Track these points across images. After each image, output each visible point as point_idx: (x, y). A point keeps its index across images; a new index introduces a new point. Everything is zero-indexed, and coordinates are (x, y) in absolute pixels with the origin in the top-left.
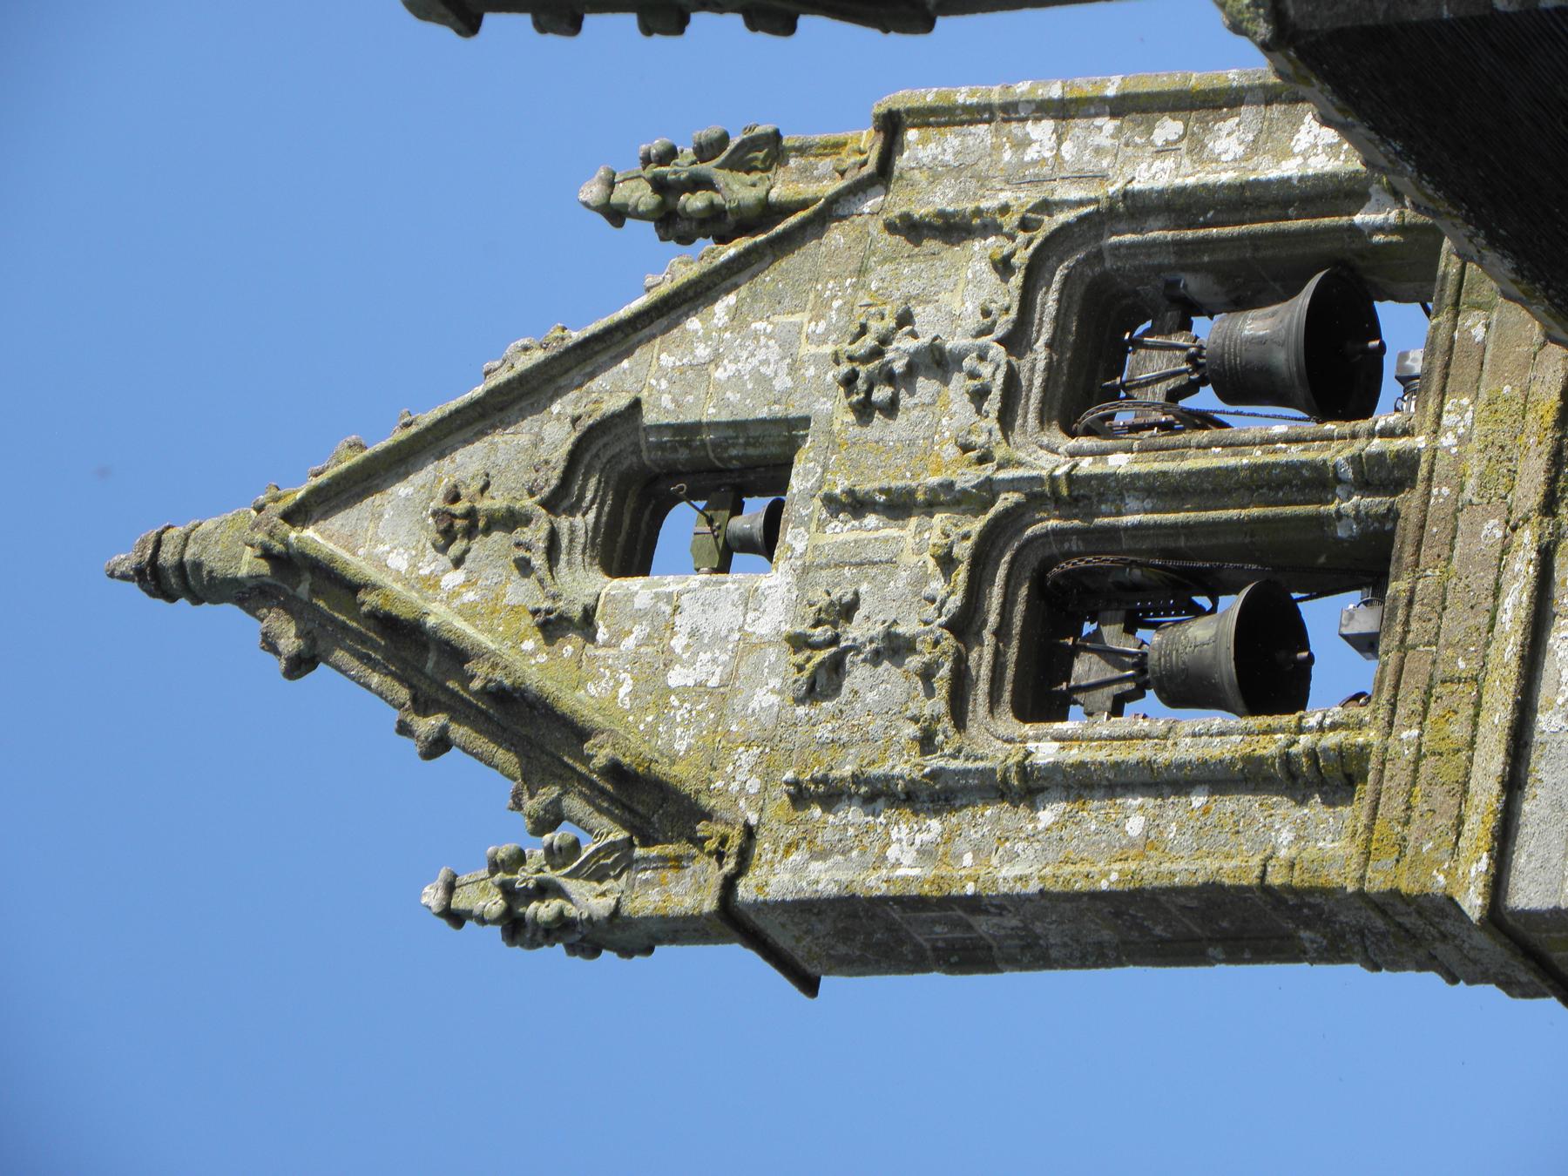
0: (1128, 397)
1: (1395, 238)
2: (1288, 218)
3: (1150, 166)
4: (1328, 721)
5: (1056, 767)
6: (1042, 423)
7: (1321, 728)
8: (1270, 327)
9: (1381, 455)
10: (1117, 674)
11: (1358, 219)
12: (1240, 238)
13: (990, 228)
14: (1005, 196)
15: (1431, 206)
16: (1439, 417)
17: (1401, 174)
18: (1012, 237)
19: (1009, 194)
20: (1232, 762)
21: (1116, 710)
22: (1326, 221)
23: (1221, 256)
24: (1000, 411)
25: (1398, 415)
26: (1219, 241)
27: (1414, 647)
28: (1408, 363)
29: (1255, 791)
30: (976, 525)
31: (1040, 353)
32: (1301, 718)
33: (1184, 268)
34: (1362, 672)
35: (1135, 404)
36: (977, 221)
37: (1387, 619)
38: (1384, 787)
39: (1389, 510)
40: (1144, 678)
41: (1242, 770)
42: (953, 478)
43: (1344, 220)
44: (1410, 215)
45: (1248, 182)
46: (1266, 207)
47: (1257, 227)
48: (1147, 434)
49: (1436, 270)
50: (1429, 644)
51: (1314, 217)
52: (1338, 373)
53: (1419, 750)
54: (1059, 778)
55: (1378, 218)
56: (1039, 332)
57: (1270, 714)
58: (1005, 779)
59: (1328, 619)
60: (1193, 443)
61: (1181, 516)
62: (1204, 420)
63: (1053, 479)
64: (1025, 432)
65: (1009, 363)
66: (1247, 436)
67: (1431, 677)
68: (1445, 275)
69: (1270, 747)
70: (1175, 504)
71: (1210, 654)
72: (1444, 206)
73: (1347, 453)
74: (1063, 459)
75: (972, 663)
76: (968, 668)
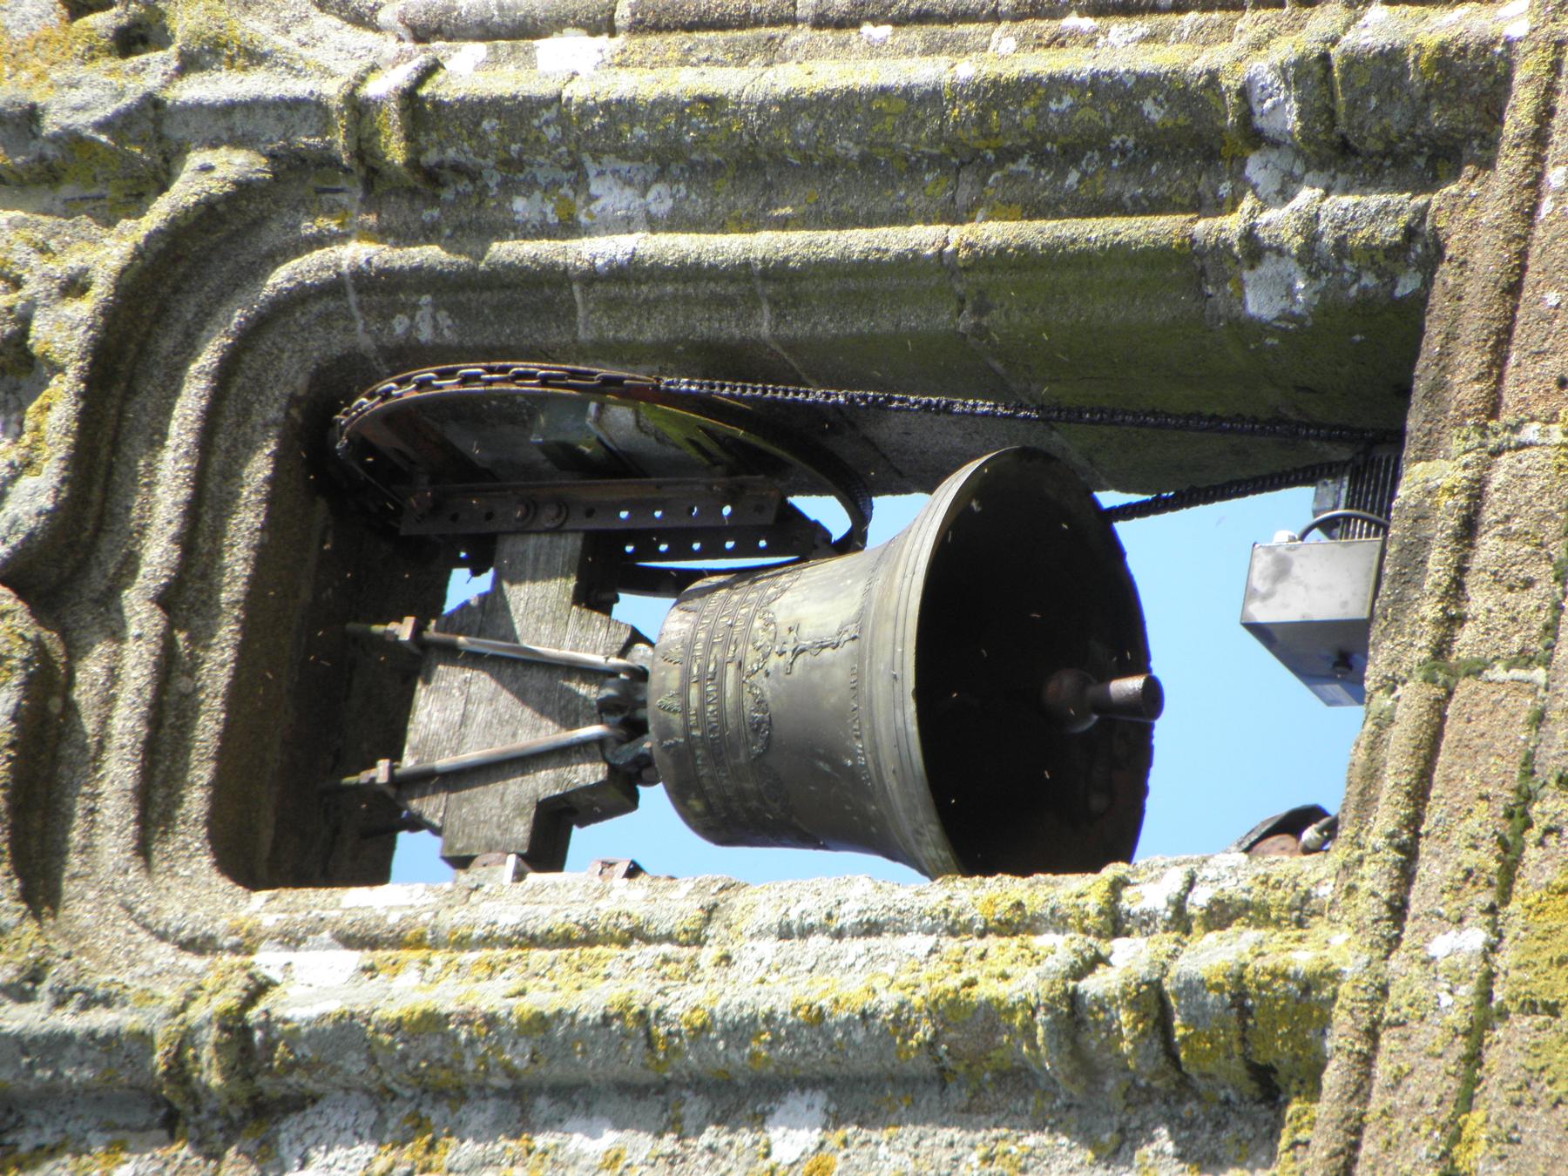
4: (1200, 898)
5: (346, 1032)
7: (1180, 920)
9: (1391, 57)
10: (550, 734)
20: (901, 1022)
21: (545, 849)
27: (1476, 669)
29: (970, 1113)
30: (109, 251)
32: (1118, 885)
34: (1314, 743)
37: (1394, 580)
38: (1375, 1106)
39: (1411, 233)
40: (631, 747)
41: (931, 1045)
42: (37, 96)
50: (1524, 659)
53: (1486, 995)
54: (354, 1064)
57: (1022, 868)
58: (179, 1069)
59: (1209, 575)
61: (763, 244)
63: (359, 109)
67: (1529, 765)
69: (1019, 975)
70: (744, 203)
71: (840, 675)
73: (1285, 49)
74: (389, 46)
75: (85, 693)
76: (71, 708)
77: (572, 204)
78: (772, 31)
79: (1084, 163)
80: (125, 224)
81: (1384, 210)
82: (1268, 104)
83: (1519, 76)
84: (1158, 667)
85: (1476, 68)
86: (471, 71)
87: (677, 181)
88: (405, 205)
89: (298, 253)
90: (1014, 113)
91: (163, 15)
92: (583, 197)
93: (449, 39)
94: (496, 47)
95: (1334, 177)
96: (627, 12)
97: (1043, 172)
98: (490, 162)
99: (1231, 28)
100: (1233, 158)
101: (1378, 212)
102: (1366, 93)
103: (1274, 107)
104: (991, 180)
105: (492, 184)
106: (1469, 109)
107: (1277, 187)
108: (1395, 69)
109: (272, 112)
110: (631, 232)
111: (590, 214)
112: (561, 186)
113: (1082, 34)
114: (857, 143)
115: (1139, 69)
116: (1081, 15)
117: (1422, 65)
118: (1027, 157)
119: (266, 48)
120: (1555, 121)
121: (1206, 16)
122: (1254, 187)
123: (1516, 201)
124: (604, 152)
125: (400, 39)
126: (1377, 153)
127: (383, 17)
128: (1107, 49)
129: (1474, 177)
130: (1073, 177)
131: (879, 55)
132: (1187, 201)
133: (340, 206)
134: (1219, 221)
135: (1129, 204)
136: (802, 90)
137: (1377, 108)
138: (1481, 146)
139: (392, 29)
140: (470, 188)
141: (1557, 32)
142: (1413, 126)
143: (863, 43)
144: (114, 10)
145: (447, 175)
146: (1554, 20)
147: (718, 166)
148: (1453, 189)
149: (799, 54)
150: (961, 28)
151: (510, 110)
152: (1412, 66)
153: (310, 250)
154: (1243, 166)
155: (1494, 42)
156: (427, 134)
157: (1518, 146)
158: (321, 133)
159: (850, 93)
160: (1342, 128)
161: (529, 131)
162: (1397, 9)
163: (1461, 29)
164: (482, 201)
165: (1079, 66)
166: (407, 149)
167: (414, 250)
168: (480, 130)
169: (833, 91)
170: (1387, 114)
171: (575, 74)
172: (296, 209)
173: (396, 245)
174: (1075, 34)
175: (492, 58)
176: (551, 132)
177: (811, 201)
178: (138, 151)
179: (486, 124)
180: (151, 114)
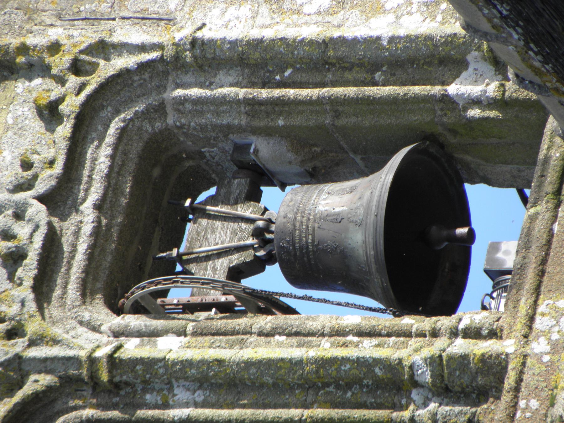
0: (185, 272)
1: (493, 114)
2: (375, 84)
3: (223, 12)
6: (84, 295)
8: (349, 204)
9: (464, 357)
11: (453, 89)
12: (320, 101)
13: (36, 68)
14: (56, 33)
15: (537, 80)
16: (532, 319)
17: (506, 42)
18: (61, 81)
19: (60, 30)
22: (417, 89)
23: (297, 121)
24: (36, 279)
25: (485, 313)
26: (297, 102)
28: (500, 255)
31: (87, 216)
33: (256, 131)
35: (192, 281)
36: (21, 59)
43: (437, 90)
44: (512, 88)
45: (331, 39)
46: (350, 69)
47: (339, 91)
48: (203, 315)
49: (537, 153)
51: (403, 84)
52: (420, 263)
55: (475, 90)
56: (87, 190)
60: (255, 329)
62: (269, 304)
63: (92, 361)
64: (63, 306)
65: (50, 225)
66: (314, 325)
68: (547, 160)
70: (230, 398)
72: (552, 81)
73: (426, 352)
74: (104, 339)
77: (167, 397)
78: (243, 337)
79: (353, 389)
80: (6, 400)
81: (460, 412)
82: (420, 372)
83: (510, 367)
84: (474, 225)
85: (495, 363)
86: (133, 348)
87: (206, 390)
88: (107, 396)
89: (67, 412)
90: (329, 370)
91: (23, 326)
92: (172, 395)
93: (127, 337)
94: (143, 340)
95: (443, 400)
96: (191, 328)
97: (338, 392)
98: (139, 381)
99: (407, 344)
100: (407, 391)
101: (458, 413)
102: (455, 370)
103: (422, 373)
104: (320, 394)
105: (139, 389)
106: (492, 378)
107: (422, 402)
108: (466, 362)
109: (61, 362)
110: (188, 408)
111: (173, 401)
112: (164, 391)
113: (354, 343)
114: (272, 378)
115: (374, 356)
116: (353, 336)
117: (475, 361)
118: (333, 386)
119: (60, 339)
120: (523, 384)
121: (398, 339)
122: (414, 402)
123: (508, 412)
124: (180, 378)
125: (109, 336)
126: (458, 392)
127: (103, 328)
128: (363, 349)
129: (493, 402)
130: (349, 394)
131: (281, 347)
132: (390, 405)
133: (83, 396)
134: (401, 413)
135: (369, 405)
136: (253, 358)
137: (459, 375)
138: (496, 391)
139: (106, 333)
140: (131, 390)
141: (524, 352)
142: (472, 382)
143: (275, 342)
144: (6, 323)
145: (123, 385)
146: (524, 347)
147: (221, 385)
148: (485, 406)
149: (252, 345)
150: (310, 338)
151: (147, 363)
152: (472, 361)
153: (72, 411)
154: (411, 393)
155: (502, 354)
156: (116, 371)
157: (509, 392)
158: (78, 369)
159: (270, 360)
160: (446, 382)
161: (153, 370)
162: (467, 340)
163: (490, 349)
164: (135, 395)
165: (353, 354)
166: (109, 376)
167: (109, 412)
168: (135, 369)
169: (264, 359)
170: (462, 378)
171: (171, 350)
172: (67, 396)
173: (103, 410)
174: (351, 342)
175: (141, 344)
176: (161, 371)
177: (254, 398)
178: (12, 374)
179: (138, 367)
180: (17, 361)
